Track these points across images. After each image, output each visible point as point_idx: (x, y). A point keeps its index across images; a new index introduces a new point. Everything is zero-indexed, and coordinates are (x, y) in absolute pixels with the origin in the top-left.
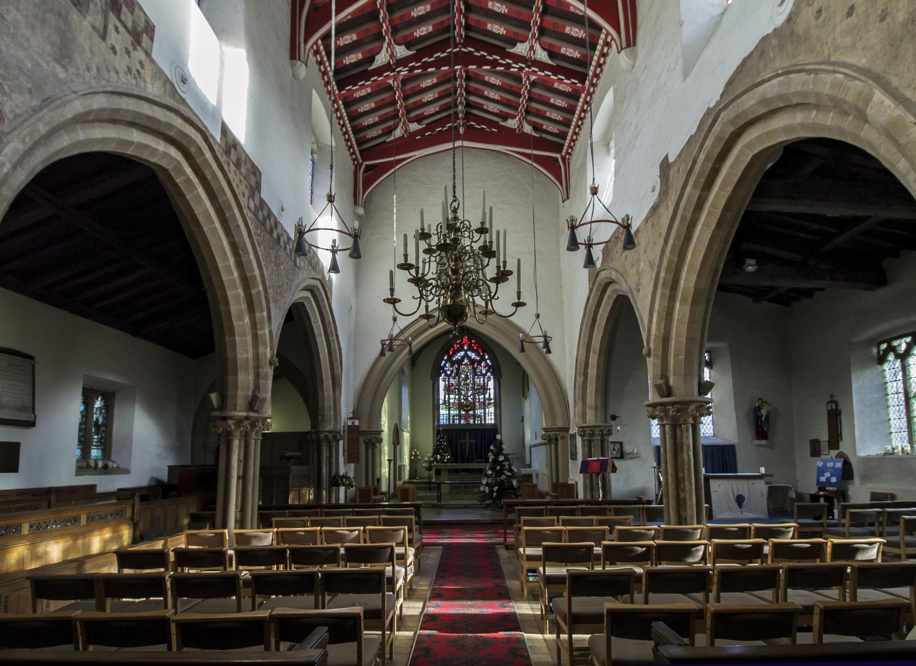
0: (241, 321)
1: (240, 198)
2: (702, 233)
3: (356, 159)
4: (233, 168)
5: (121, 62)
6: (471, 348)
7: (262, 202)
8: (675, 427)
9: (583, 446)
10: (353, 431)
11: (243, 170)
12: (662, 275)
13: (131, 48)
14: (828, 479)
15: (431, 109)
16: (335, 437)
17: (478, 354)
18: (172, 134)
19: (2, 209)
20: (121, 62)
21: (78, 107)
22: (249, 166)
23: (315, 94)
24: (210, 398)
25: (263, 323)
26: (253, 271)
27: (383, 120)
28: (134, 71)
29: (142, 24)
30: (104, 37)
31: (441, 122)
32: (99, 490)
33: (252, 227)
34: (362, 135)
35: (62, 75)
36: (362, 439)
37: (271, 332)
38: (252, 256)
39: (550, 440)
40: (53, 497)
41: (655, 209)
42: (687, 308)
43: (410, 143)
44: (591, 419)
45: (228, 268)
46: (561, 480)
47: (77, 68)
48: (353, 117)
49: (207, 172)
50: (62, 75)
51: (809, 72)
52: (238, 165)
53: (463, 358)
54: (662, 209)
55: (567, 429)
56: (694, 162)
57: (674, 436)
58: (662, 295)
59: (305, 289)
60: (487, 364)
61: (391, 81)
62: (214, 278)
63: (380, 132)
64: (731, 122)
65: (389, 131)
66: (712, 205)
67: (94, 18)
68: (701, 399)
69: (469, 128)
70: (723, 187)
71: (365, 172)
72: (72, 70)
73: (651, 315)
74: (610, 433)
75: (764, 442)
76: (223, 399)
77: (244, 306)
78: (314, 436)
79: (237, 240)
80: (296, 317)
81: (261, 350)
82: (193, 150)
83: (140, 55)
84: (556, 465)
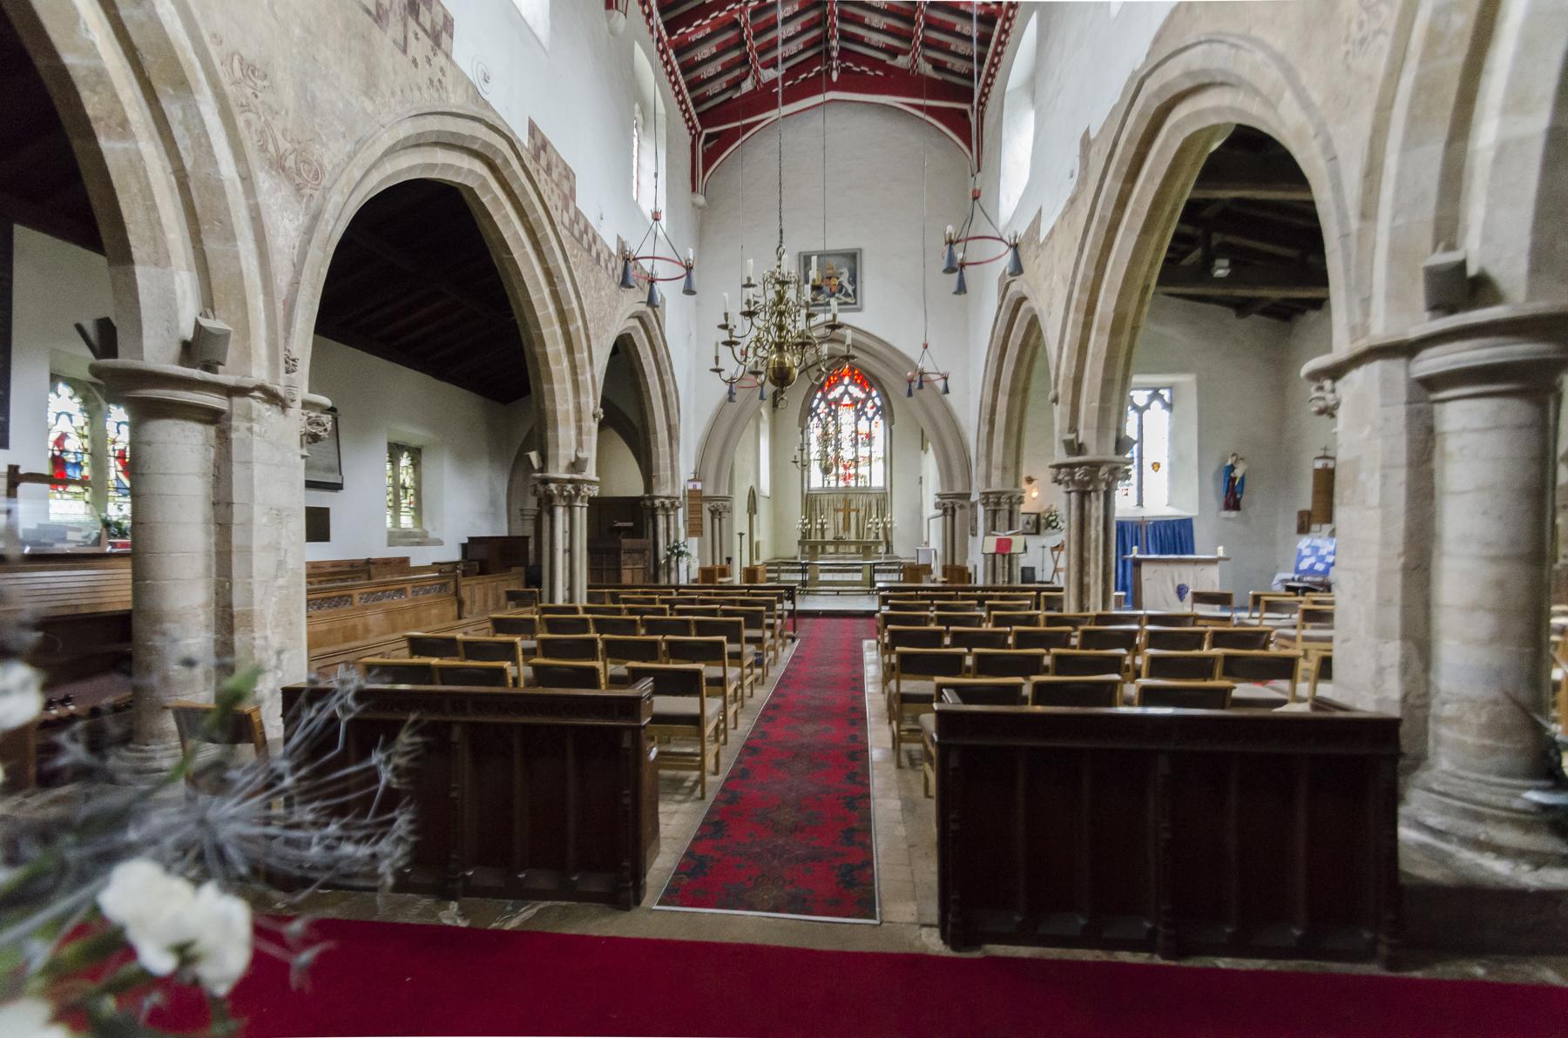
0: (559, 366)
1: (553, 212)
2: (1125, 241)
3: (694, 127)
4: (543, 175)
5: (423, 74)
6: (853, 382)
7: (578, 212)
8: (1084, 495)
9: (986, 520)
10: (695, 497)
11: (555, 175)
12: (1076, 295)
13: (431, 54)
14: (1312, 565)
15: (794, 47)
16: (673, 504)
17: (863, 390)
18: (476, 147)
19: (879, 838)
20: (423, 74)
21: (386, 141)
22: (561, 168)
23: (638, 49)
24: (528, 458)
25: (583, 366)
26: (570, 303)
27: (728, 68)
28: (436, 83)
29: (440, 21)
30: (405, 51)
31: (806, 65)
32: (413, 564)
33: (567, 247)
34: (700, 91)
35: (370, 108)
36: (706, 506)
37: (593, 377)
38: (569, 284)
39: (945, 511)
40: (372, 568)
41: (1072, 201)
42: (1105, 339)
43: (764, 99)
44: (996, 485)
45: (543, 300)
46: (957, 563)
47: (383, 97)
48: (687, 68)
49: (515, 186)
50: (370, 108)
51: (1233, 45)
52: (548, 171)
53: (842, 396)
54: (1079, 203)
55: (967, 496)
56: (1115, 145)
57: (1081, 507)
58: (1075, 321)
59: (632, 317)
60: (875, 405)
61: (736, 16)
62: (528, 315)
63: (714, 50)
64: (1157, 94)
65: (736, 84)
66: (1136, 202)
67: (394, 30)
68: (1118, 458)
69: (844, 72)
70: (1149, 178)
71: (706, 142)
72: (378, 100)
73: (1061, 348)
74: (1020, 500)
75: (1233, 514)
76: (544, 458)
77: (562, 347)
78: (648, 503)
79: (551, 265)
80: (623, 352)
81: (583, 400)
82: (498, 162)
83: (440, 60)
84: (952, 541)
